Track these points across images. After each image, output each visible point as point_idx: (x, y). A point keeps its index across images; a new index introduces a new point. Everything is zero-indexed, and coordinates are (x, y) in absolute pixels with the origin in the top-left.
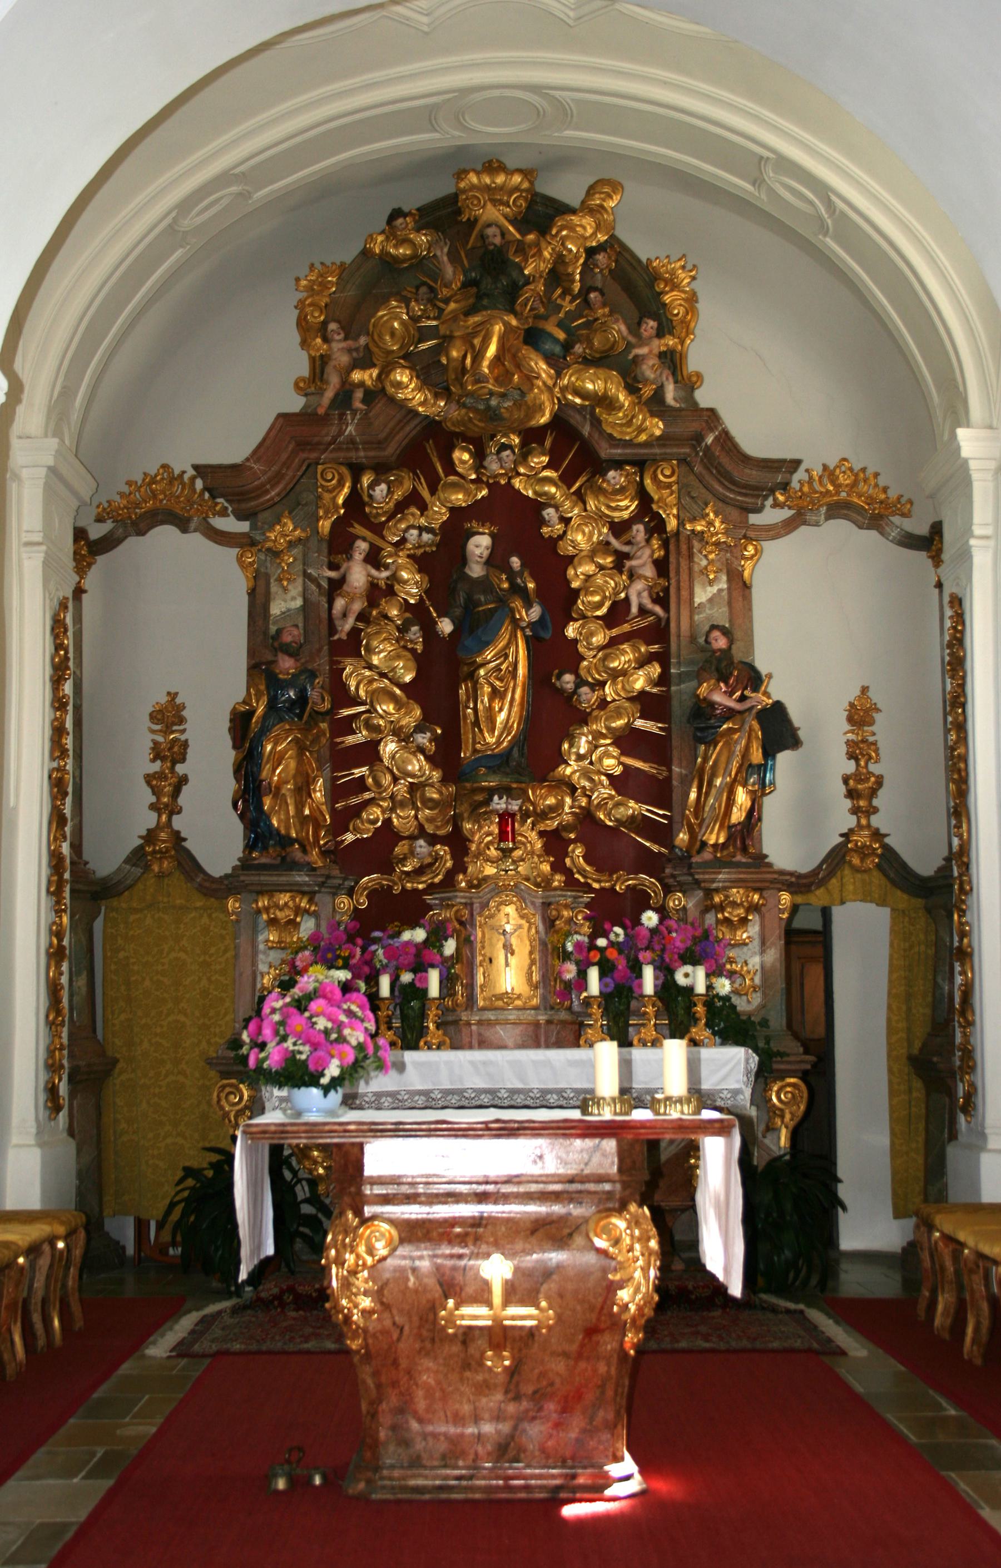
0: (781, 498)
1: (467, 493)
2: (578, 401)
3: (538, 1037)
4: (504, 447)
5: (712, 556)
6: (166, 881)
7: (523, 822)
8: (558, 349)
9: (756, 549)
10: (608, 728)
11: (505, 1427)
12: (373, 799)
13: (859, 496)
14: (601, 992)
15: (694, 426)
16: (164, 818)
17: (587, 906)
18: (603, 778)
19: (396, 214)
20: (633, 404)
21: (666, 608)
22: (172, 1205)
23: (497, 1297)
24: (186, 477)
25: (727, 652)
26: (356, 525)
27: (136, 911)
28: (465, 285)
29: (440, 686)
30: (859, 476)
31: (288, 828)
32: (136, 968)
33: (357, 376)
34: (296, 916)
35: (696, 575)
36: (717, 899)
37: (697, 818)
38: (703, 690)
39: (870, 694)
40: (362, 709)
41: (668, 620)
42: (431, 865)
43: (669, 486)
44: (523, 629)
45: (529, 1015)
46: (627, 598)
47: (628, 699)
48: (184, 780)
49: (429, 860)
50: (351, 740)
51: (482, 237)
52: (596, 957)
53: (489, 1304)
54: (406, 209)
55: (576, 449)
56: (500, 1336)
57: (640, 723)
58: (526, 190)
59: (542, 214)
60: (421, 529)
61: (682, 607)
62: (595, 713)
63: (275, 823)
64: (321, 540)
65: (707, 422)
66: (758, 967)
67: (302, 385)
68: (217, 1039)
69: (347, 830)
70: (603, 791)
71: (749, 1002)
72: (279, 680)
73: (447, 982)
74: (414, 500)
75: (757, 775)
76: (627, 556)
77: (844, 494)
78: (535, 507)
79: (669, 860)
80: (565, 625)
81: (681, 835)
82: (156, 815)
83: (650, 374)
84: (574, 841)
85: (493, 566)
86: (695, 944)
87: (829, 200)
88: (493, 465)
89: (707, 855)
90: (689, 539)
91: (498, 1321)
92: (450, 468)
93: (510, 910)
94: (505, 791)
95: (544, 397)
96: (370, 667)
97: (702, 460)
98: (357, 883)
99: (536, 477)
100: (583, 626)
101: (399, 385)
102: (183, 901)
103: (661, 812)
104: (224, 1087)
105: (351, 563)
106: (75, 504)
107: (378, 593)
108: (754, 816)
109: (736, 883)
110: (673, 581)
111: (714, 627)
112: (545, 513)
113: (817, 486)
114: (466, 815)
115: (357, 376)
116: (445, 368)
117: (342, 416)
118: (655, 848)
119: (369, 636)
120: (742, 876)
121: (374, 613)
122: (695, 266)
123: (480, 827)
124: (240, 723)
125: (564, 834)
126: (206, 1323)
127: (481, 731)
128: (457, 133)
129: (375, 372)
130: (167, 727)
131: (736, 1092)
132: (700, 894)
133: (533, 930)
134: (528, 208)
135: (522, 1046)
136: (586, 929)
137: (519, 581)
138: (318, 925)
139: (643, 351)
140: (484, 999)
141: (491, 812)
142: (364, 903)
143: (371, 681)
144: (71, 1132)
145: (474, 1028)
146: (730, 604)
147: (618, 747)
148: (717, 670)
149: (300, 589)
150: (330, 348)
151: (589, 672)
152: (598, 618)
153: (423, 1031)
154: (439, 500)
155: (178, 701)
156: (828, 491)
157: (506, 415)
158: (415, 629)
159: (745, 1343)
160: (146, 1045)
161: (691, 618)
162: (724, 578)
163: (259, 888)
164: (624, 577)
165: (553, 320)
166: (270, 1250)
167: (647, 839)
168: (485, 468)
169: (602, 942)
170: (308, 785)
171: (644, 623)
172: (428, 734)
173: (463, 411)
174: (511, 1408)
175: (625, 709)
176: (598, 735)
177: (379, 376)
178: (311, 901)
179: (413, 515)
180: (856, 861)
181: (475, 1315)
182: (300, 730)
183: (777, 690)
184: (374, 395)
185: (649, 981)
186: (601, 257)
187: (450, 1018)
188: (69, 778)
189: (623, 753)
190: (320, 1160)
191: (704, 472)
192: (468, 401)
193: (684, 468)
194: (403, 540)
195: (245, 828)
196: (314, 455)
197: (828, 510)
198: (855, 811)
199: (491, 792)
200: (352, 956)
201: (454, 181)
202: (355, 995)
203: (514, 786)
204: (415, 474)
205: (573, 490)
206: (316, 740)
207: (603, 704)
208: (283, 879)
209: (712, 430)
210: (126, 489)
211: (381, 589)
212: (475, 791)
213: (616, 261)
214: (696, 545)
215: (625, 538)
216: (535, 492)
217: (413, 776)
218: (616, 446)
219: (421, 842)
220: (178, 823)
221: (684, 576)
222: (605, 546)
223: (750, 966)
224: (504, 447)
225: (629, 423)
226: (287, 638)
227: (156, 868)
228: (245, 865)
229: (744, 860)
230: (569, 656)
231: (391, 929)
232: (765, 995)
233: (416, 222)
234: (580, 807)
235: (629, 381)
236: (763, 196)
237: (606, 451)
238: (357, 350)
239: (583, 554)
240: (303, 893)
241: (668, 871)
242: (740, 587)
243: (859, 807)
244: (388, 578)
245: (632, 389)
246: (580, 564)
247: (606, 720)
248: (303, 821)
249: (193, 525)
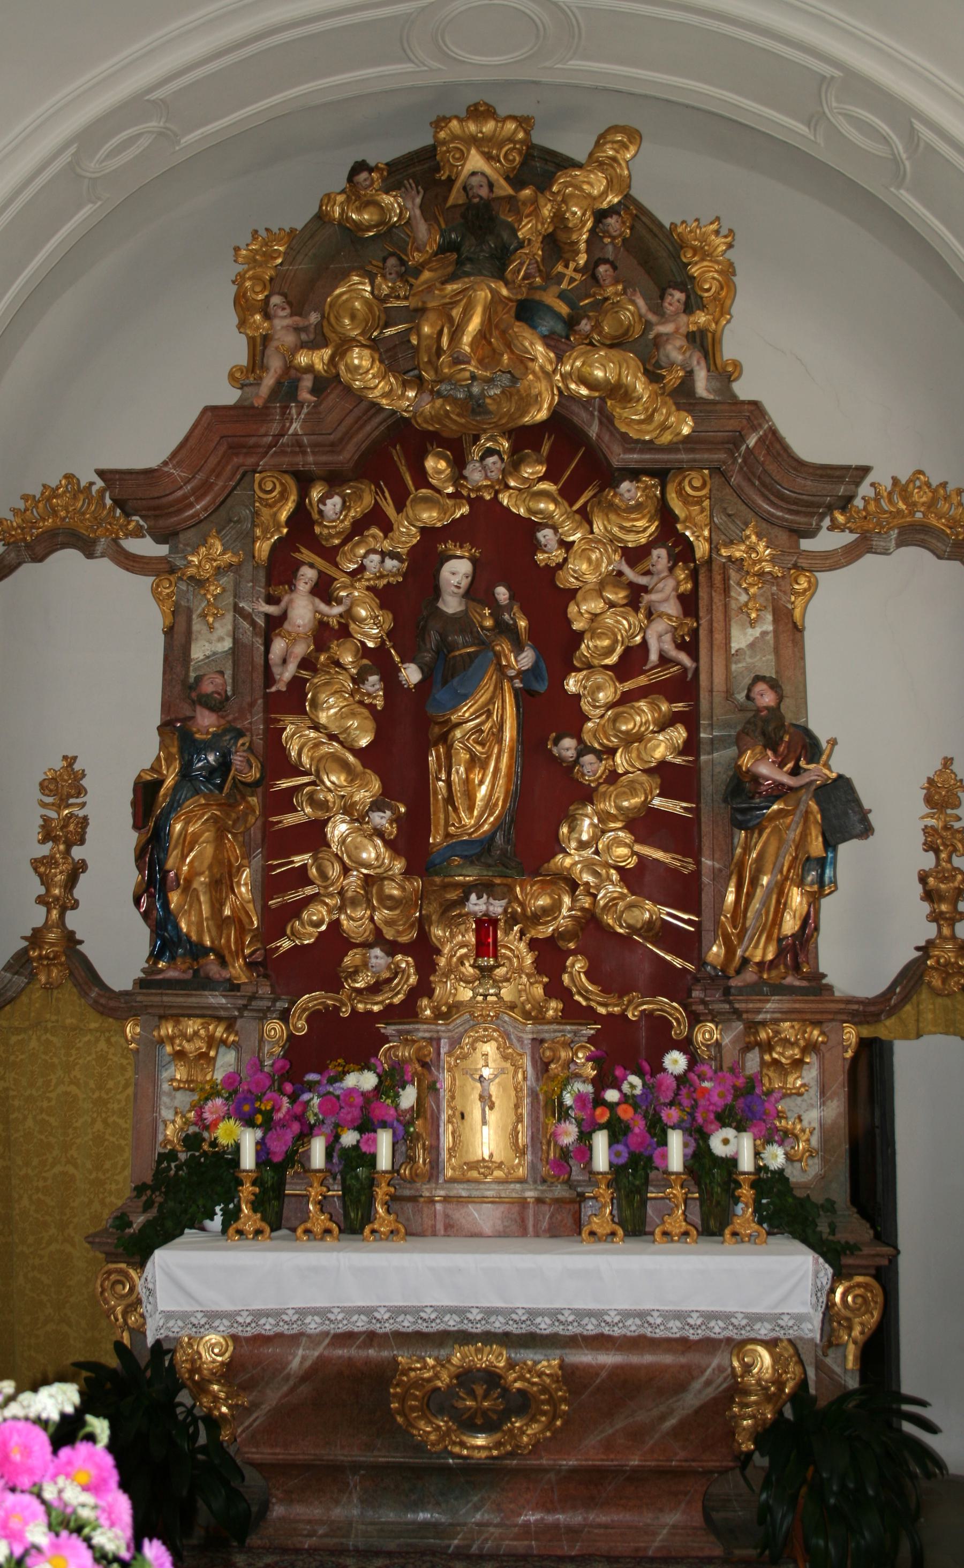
0: (841, 518)
1: (444, 510)
2: (584, 391)
4: (489, 452)
5: (752, 591)
6: (55, 992)
7: (507, 932)
8: (559, 328)
9: (809, 582)
10: (619, 808)
12: (317, 894)
13: (940, 518)
14: (611, 1165)
16: (55, 914)
17: (591, 1040)
18: (613, 871)
19: (360, 167)
20: (654, 396)
21: (695, 657)
24: (94, 489)
25: (775, 712)
26: (303, 550)
27: (18, 1031)
28: (444, 249)
29: (404, 749)
30: (939, 493)
31: (200, 933)
32: (16, 1103)
33: (303, 359)
34: (209, 1047)
35: (733, 613)
36: (763, 1035)
37: (735, 927)
38: (746, 760)
39: (955, 767)
40: (306, 779)
41: (697, 671)
42: (389, 980)
43: (699, 501)
44: (511, 679)
45: (514, 1190)
46: (644, 640)
47: (644, 771)
48: (79, 868)
49: (386, 975)
50: (290, 819)
52: (603, 1115)
54: (372, 163)
55: (578, 455)
57: (658, 802)
58: (521, 142)
59: (539, 167)
60: (383, 554)
61: (715, 654)
62: (603, 789)
63: (183, 926)
64: (256, 567)
65: (749, 418)
66: (816, 1124)
67: (238, 375)
68: (113, 1199)
69: (283, 934)
70: (611, 888)
71: (803, 1171)
72: (194, 741)
74: (376, 518)
75: (817, 873)
76: (645, 589)
77: (919, 515)
78: (527, 529)
79: (697, 980)
80: (565, 676)
81: (715, 949)
82: (44, 909)
83: (677, 357)
84: (574, 953)
85: (473, 600)
86: (736, 1098)
87: (912, 129)
88: (475, 474)
89: (750, 976)
90: (724, 567)
92: (422, 479)
93: (490, 1048)
94: (485, 888)
95: (542, 386)
96: (316, 727)
97: (741, 468)
98: (293, 1003)
99: (530, 493)
100: (587, 678)
102: (74, 1021)
103: (686, 917)
104: (109, 1273)
105: (294, 596)
107: (326, 634)
108: (809, 926)
109: (788, 1015)
110: (703, 622)
111: (758, 679)
112: (540, 535)
113: (885, 504)
114: (434, 917)
115: (303, 359)
116: (416, 349)
117: (285, 408)
118: (678, 963)
119: (316, 688)
120: (797, 1006)
121: (322, 658)
122: (731, 231)
123: (453, 936)
124: (146, 793)
125: (561, 944)
127: (456, 810)
128: (436, 65)
129: (327, 353)
130: (61, 800)
131: (799, 1319)
132: (740, 1026)
133: (520, 1076)
134: (523, 164)
137: (506, 616)
138: (239, 1060)
140: (453, 1169)
141: (467, 914)
142: (301, 1026)
143: (317, 745)
145: (439, 1207)
146: (776, 650)
147: (632, 832)
148: (764, 734)
149: (230, 627)
150: (272, 327)
151: (595, 736)
152: (606, 667)
153: (368, 1218)
154: (407, 518)
155: (77, 767)
156: (899, 511)
157: (493, 407)
158: (373, 679)
160: (25, 1202)
161: (727, 667)
162: (769, 617)
163: (161, 1012)
164: (641, 616)
165: (554, 290)
167: (668, 951)
168: (465, 478)
169: (612, 1095)
170: (231, 877)
171: (665, 675)
172: (388, 813)
173: (439, 402)
175: (641, 784)
176: (605, 817)
177: (332, 358)
178: (230, 1028)
179: (374, 537)
180: (937, 982)
182: (220, 806)
183: (840, 764)
184: (326, 383)
185: (676, 1151)
186: (612, 221)
187: (407, 1193)
189: (637, 841)
190: (222, 1395)
191: (744, 484)
192: (443, 387)
193: (718, 480)
194: (362, 568)
195: (152, 931)
196: (251, 460)
197: (900, 534)
198: (935, 917)
199: (467, 889)
200: (276, 1108)
201: (432, 130)
202: (83, 1448)
203: (498, 881)
204: (378, 486)
205: (576, 507)
207: (613, 777)
208: (193, 1000)
209: (754, 429)
210: (21, 505)
211: (332, 629)
212: (446, 887)
213: (632, 228)
214: (734, 575)
215: (642, 567)
216: (529, 510)
217: (368, 866)
218: (632, 451)
219: (377, 951)
220: (73, 920)
221: (718, 615)
223: (805, 1123)
224: (489, 452)
225: (649, 419)
226: (208, 687)
227: (43, 979)
229: (797, 983)
230: (570, 716)
232: (825, 1161)
233: (384, 180)
234: (582, 909)
235: (649, 367)
236: (820, 140)
237: (619, 457)
238: (305, 329)
239: (588, 587)
240: (219, 1019)
241: (695, 994)
242: (790, 630)
243: (941, 913)
244: (341, 615)
245: (653, 376)
246: (585, 599)
247: (617, 796)
248: (221, 923)
249: (99, 549)
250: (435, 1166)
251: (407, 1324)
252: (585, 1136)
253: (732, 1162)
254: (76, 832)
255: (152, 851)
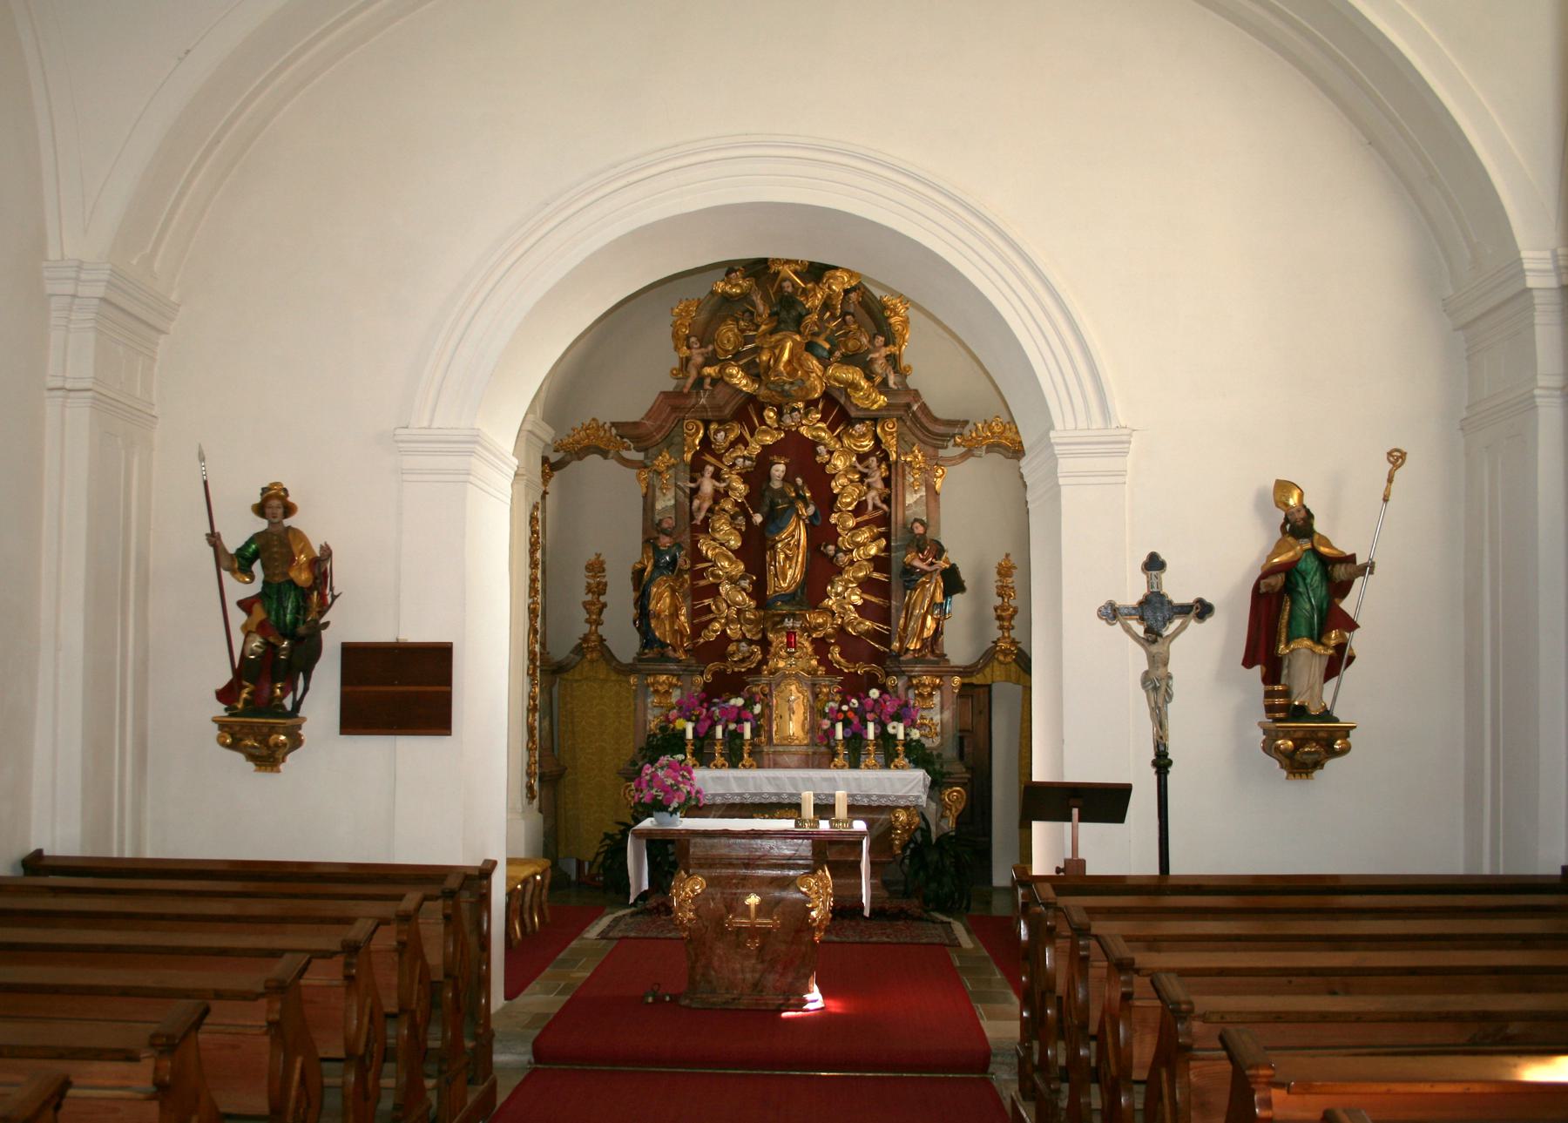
3: (810, 762)
4: (794, 410)
8: (825, 354)
11: (757, 975)
15: (903, 400)
21: (889, 506)
22: (598, 854)
23: (753, 914)
29: (755, 550)
33: (708, 370)
48: (604, 605)
50: (703, 583)
51: (781, 288)
52: (841, 716)
53: (748, 917)
56: (753, 932)
57: (876, 575)
60: (745, 458)
73: (755, 731)
74: (741, 440)
83: (879, 370)
88: (787, 420)
89: (909, 656)
91: (753, 926)
92: (762, 422)
93: (793, 688)
94: (793, 616)
99: (813, 427)
101: (731, 376)
106: (542, 445)
107: (718, 496)
108: (938, 632)
109: (926, 673)
111: (916, 520)
124: (638, 575)
126: (617, 921)
131: (918, 797)
135: (798, 767)
136: (838, 698)
139: (876, 355)
142: (709, 677)
144: (540, 811)
153: (742, 758)
159: (908, 940)
165: (823, 336)
166: (645, 886)
169: (845, 708)
174: (759, 967)
181: (742, 922)
186: (853, 295)
188: (539, 607)
194: (734, 464)
206: (682, 585)
207: (852, 563)
222: (853, 468)
224: (794, 410)
226: (665, 525)
228: (640, 658)
230: (832, 534)
231: (724, 697)
237: (853, 413)
245: (869, 378)
248: (675, 632)
250: (770, 739)
251: (757, 800)
252: (833, 726)
253: (895, 736)
254: (601, 589)
255: (642, 601)
